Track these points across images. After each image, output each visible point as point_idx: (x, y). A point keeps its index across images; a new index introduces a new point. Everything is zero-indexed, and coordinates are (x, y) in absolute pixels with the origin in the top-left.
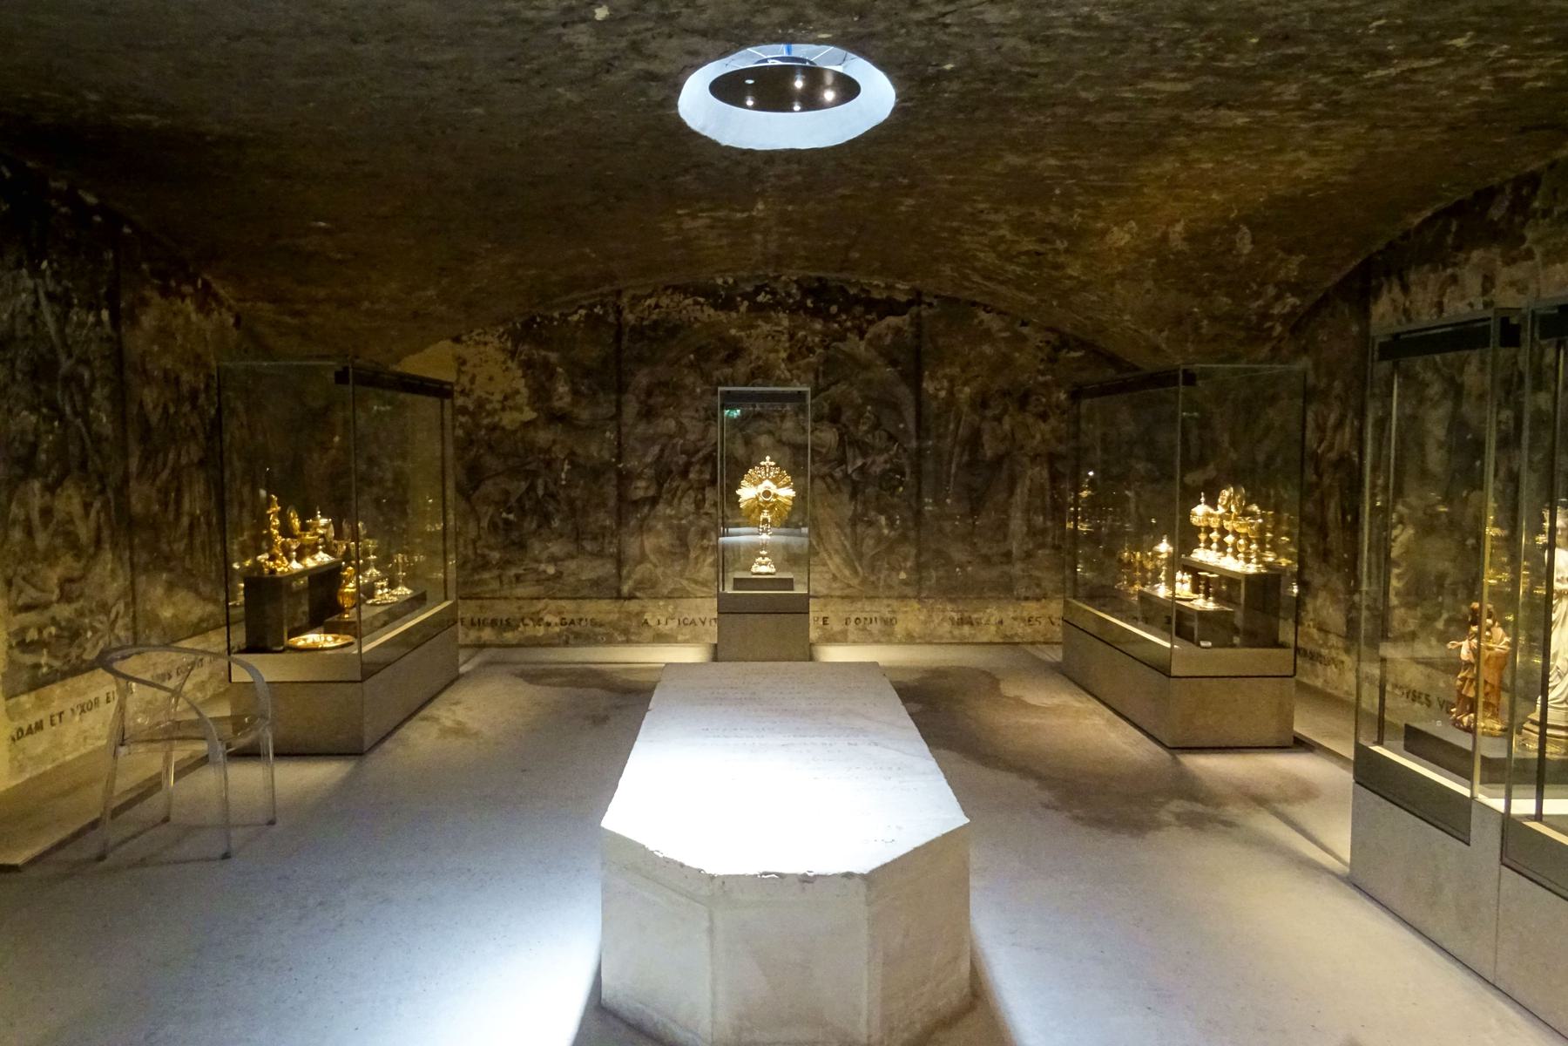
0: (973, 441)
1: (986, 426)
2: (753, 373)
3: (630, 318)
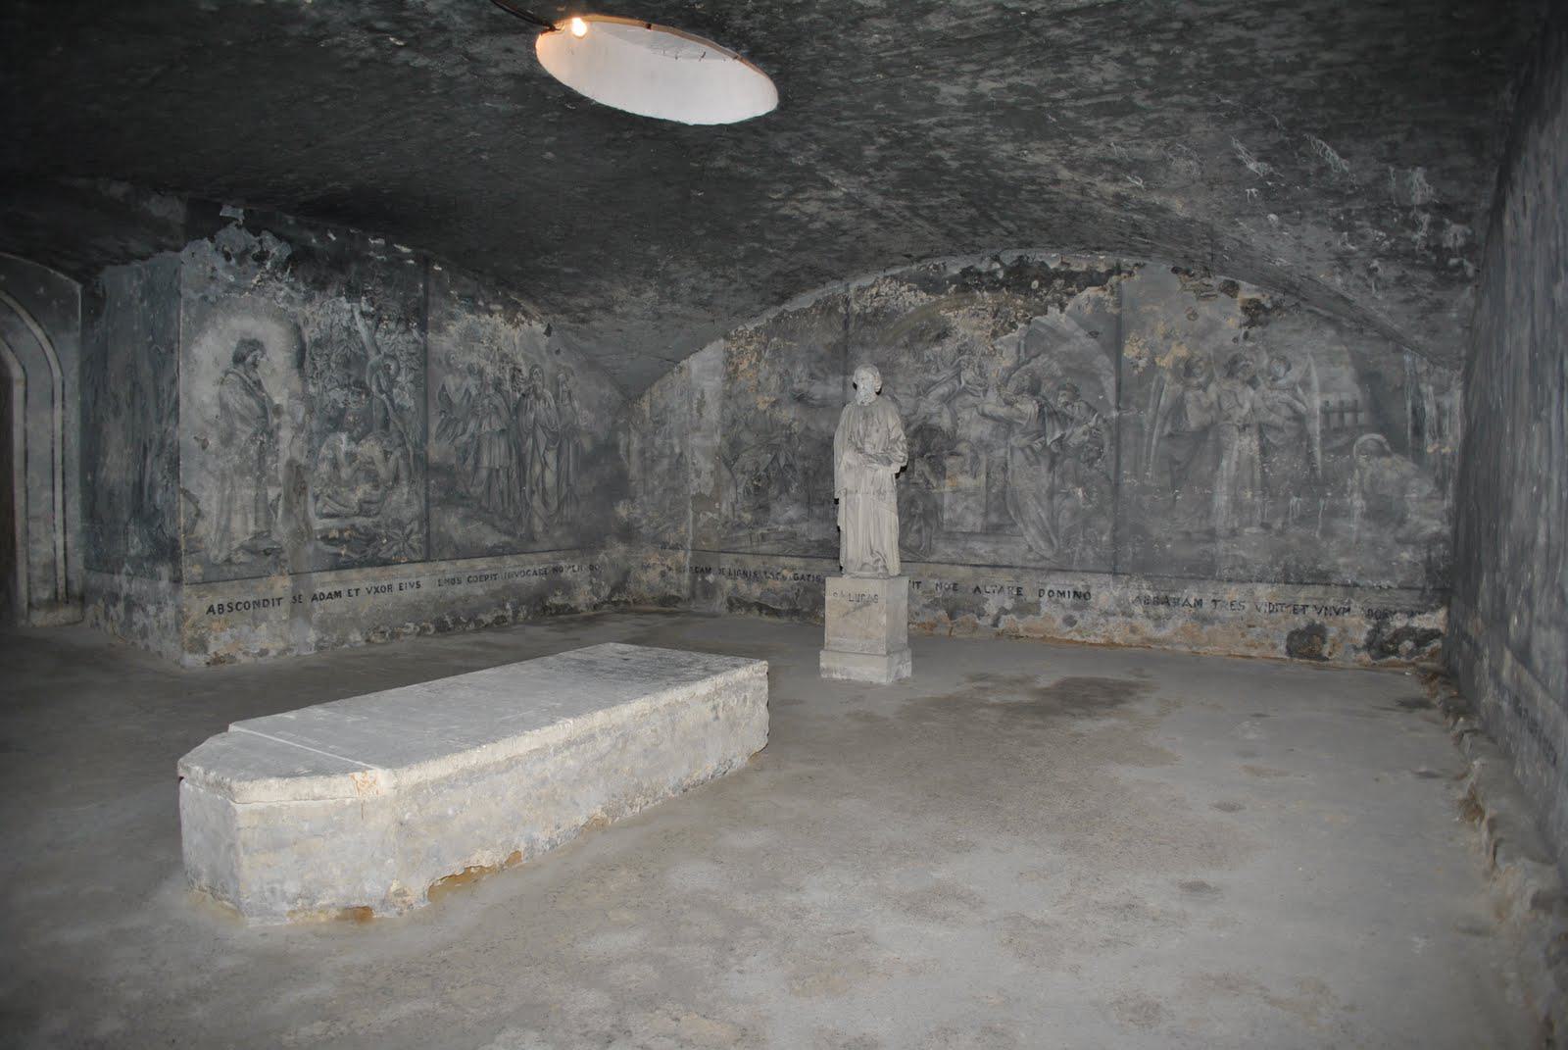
0: (1178, 408)
1: (1190, 395)
2: (959, 351)
3: (856, 307)
